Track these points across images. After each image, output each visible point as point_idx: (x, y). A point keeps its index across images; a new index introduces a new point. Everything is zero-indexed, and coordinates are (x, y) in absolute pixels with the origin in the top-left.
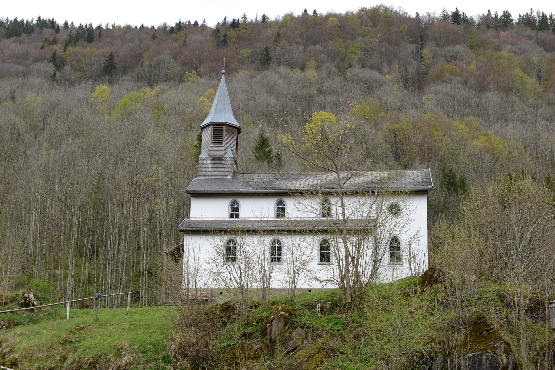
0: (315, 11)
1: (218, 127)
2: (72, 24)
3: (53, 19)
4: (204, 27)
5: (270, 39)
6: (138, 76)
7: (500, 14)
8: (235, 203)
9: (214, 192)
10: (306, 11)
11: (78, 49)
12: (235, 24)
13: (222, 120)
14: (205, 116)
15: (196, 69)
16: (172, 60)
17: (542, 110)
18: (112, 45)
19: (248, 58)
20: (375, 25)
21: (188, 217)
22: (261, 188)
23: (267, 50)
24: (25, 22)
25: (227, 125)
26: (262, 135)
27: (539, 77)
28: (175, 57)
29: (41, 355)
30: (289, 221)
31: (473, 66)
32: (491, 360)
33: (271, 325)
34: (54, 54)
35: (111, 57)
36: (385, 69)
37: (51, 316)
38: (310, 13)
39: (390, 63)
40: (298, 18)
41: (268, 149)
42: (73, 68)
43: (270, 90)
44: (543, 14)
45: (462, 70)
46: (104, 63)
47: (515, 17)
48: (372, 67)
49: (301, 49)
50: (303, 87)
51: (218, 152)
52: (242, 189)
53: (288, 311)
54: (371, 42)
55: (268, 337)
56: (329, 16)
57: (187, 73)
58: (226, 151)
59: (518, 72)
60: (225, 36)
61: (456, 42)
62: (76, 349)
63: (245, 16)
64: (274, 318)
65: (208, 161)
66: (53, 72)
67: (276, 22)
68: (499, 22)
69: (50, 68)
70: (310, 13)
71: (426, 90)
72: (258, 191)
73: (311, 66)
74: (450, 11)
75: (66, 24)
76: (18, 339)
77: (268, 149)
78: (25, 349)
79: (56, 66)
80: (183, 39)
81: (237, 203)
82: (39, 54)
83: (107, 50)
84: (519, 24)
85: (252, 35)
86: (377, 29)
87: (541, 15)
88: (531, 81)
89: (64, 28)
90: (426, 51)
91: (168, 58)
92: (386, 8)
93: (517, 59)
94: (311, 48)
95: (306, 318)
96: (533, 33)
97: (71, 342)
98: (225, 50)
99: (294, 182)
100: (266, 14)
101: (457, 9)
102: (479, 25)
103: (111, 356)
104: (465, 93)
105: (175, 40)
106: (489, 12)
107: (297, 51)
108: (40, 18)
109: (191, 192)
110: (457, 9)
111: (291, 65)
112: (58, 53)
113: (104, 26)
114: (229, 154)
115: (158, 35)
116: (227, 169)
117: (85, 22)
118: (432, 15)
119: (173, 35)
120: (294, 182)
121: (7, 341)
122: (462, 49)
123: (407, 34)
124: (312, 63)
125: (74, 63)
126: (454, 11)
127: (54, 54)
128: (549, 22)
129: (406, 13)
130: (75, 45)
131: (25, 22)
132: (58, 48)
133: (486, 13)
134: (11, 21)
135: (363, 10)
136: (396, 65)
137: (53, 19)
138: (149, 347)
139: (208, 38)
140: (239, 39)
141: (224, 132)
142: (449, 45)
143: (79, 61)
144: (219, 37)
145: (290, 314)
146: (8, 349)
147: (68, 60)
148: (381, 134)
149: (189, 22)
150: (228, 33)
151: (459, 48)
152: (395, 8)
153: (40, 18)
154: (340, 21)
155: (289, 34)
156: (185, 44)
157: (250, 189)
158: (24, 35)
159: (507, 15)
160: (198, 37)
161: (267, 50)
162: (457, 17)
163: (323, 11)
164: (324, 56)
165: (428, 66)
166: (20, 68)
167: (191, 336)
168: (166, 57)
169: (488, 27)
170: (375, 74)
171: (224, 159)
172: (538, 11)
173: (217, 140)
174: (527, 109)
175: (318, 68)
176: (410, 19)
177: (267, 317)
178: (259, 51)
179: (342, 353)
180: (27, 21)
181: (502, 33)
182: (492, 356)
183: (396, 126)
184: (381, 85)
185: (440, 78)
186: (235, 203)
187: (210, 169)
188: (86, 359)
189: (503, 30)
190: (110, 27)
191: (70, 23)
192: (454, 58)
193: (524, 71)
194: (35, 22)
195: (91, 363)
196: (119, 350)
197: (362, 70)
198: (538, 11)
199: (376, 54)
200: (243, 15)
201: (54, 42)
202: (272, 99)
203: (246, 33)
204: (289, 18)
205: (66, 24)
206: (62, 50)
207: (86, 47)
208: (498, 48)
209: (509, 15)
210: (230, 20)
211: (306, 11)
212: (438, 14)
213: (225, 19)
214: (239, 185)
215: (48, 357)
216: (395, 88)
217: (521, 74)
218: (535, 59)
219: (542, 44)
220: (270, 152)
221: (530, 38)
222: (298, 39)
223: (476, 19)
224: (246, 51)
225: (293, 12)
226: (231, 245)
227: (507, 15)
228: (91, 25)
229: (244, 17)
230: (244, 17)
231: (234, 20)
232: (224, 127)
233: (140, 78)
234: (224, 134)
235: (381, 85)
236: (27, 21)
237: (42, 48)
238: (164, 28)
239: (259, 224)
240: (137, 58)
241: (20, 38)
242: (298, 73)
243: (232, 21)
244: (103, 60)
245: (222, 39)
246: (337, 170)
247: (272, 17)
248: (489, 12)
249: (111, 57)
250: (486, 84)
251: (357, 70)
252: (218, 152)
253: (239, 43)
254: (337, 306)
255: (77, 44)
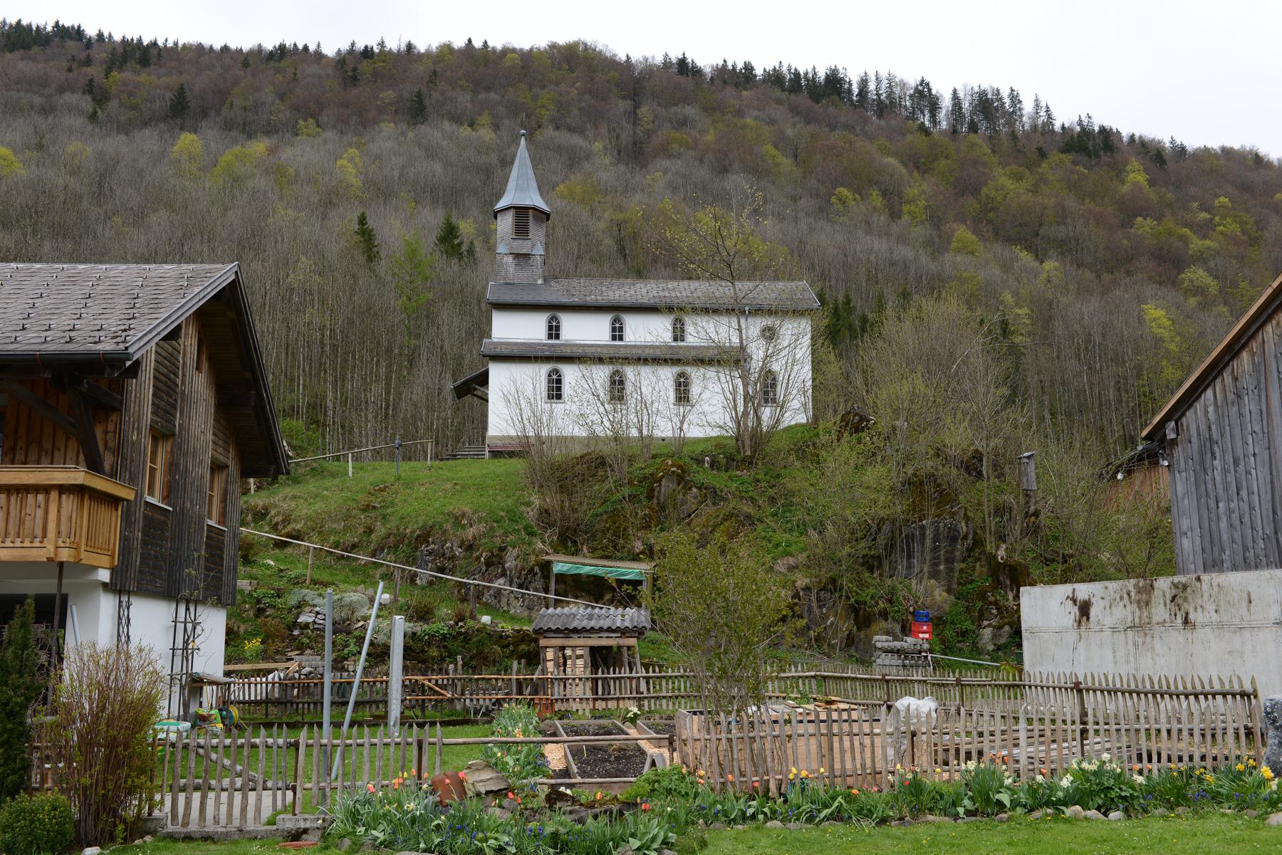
0: (486, 42)
1: (521, 212)
2: (110, 35)
3: (79, 27)
4: (318, 55)
5: (422, 78)
6: (225, 122)
7: (740, 66)
8: (554, 318)
9: (527, 302)
10: (470, 41)
11: (127, 75)
12: (367, 53)
13: (528, 202)
14: (499, 196)
15: (313, 116)
16: (277, 101)
17: (803, 203)
18: (181, 73)
19: (391, 104)
20: (571, 70)
21: (490, 336)
22: (591, 299)
23: (419, 95)
24: (34, 27)
25: (535, 209)
26: (448, 220)
27: (796, 156)
28: (281, 97)
29: (339, 526)
30: (566, 345)
31: (710, 137)
32: (950, 528)
33: (660, 485)
34: (91, 81)
35: (181, 91)
36: (590, 134)
37: (317, 472)
38: (478, 44)
39: (596, 126)
40: (460, 51)
41: (456, 241)
42: (122, 104)
43: (431, 152)
44: (796, 70)
45: (696, 141)
46: (171, 100)
47: (759, 71)
48: (570, 129)
49: (468, 96)
50: (479, 153)
51: (523, 247)
52: (565, 300)
53: (680, 467)
54: (568, 93)
55: (655, 501)
56: (506, 51)
57: (301, 122)
58: (533, 246)
59: (769, 149)
60: (355, 69)
61: (685, 100)
62: (384, 518)
63: (383, 42)
64: (663, 476)
65: (510, 260)
66: (91, 110)
67: (428, 54)
68: (738, 77)
69: (86, 103)
70: (478, 44)
71: (650, 167)
72: (588, 304)
73: (484, 122)
74: (675, 56)
75: (100, 35)
76: (293, 504)
77: (456, 241)
78: (309, 518)
79: (94, 99)
80: (291, 70)
81: (556, 319)
82: (66, 80)
83: (174, 80)
84: (764, 81)
85: (395, 71)
86: (575, 75)
87: (793, 71)
88: (786, 162)
89: (98, 40)
90: (644, 111)
91: (270, 98)
92: (585, 45)
93: (767, 131)
94: (482, 96)
95: (705, 476)
96: (784, 95)
97: (374, 507)
98: (355, 91)
99: (633, 292)
100: (412, 42)
101: (319, 45)
102: (712, 79)
103: (448, 526)
104: (703, 173)
105: (279, 71)
106: (725, 61)
107: (464, 99)
108: (57, 23)
109: (494, 301)
110: (319, 45)
111: (457, 119)
112: (96, 80)
113: (160, 43)
114: (539, 250)
115: (251, 62)
116: (535, 272)
117: (132, 34)
118: (650, 60)
119: (272, 64)
120: (633, 292)
121: (276, 506)
122: (693, 111)
123: (617, 85)
124: (485, 119)
125: (124, 96)
126: (680, 56)
127: (91, 81)
128: (803, 82)
129: (615, 55)
130: (121, 69)
131: (34, 27)
132: (95, 71)
133: (721, 63)
134: (11, 25)
135: (553, 46)
136: (604, 129)
137: (79, 27)
138: (502, 514)
139: (330, 71)
140: (376, 75)
141: (531, 218)
142: (677, 105)
143: (131, 94)
144: (346, 71)
145: (684, 471)
146: (280, 518)
147: (113, 90)
148: (601, 225)
149: (295, 45)
150: (360, 67)
151: (689, 111)
152: (600, 47)
153: (57, 23)
154: (522, 60)
155: (449, 73)
156: (295, 78)
157: (576, 300)
158: (36, 49)
159: (748, 68)
160: (315, 69)
161: (419, 95)
162: (683, 66)
163: (497, 43)
164: (501, 110)
165: (649, 133)
166: (38, 100)
167: (552, 500)
168: (268, 96)
169: (725, 82)
170: (576, 140)
171: (532, 258)
172: (790, 66)
173: (521, 230)
174: (784, 200)
175: (496, 127)
176: (619, 64)
177: (652, 475)
178: (406, 95)
179: (760, 520)
180: (38, 27)
181: (745, 93)
182: (951, 524)
183: (620, 216)
184: (589, 156)
185: (665, 150)
186: (554, 318)
187: (511, 270)
188: (408, 531)
189: (746, 89)
190: (170, 44)
191: (106, 34)
192: (683, 123)
193: (776, 147)
194: (49, 29)
195: (419, 536)
196: (456, 518)
197: (556, 133)
198: (790, 66)
199: (575, 111)
200: (379, 40)
201: (88, 62)
202: (438, 168)
203: (384, 68)
204: (447, 49)
205: (100, 35)
206: (102, 75)
207: (139, 74)
208: (739, 113)
209: (752, 69)
210: (360, 46)
211: (470, 41)
212: (659, 59)
213: (353, 44)
214: (555, 293)
215: (347, 529)
216: (607, 160)
217: (773, 151)
218: (790, 132)
219: (795, 110)
220: (460, 245)
221: (779, 101)
222: (462, 82)
223: (708, 70)
224: (388, 95)
225: (452, 40)
226: (682, 380)
227: (748, 68)
228: (140, 40)
229: (382, 44)
230: (382, 44)
231: (366, 47)
232: (531, 212)
233: (228, 126)
234: (531, 224)
235: (589, 156)
236: (38, 27)
237: (70, 70)
238: (258, 52)
239: (593, 350)
240: (222, 95)
241: (31, 52)
242: (465, 131)
243: (363, 47)
244: (169, 95)
245: (350, 74)
246: (733, 278)
247: (421, 47)
248: (725, 61)
249: (181, 91)
250: (727, 163)
251: (549, 132)
252: (523, 247)
253: (375, 81)
254: (733, 460)
255: (124, 67)
